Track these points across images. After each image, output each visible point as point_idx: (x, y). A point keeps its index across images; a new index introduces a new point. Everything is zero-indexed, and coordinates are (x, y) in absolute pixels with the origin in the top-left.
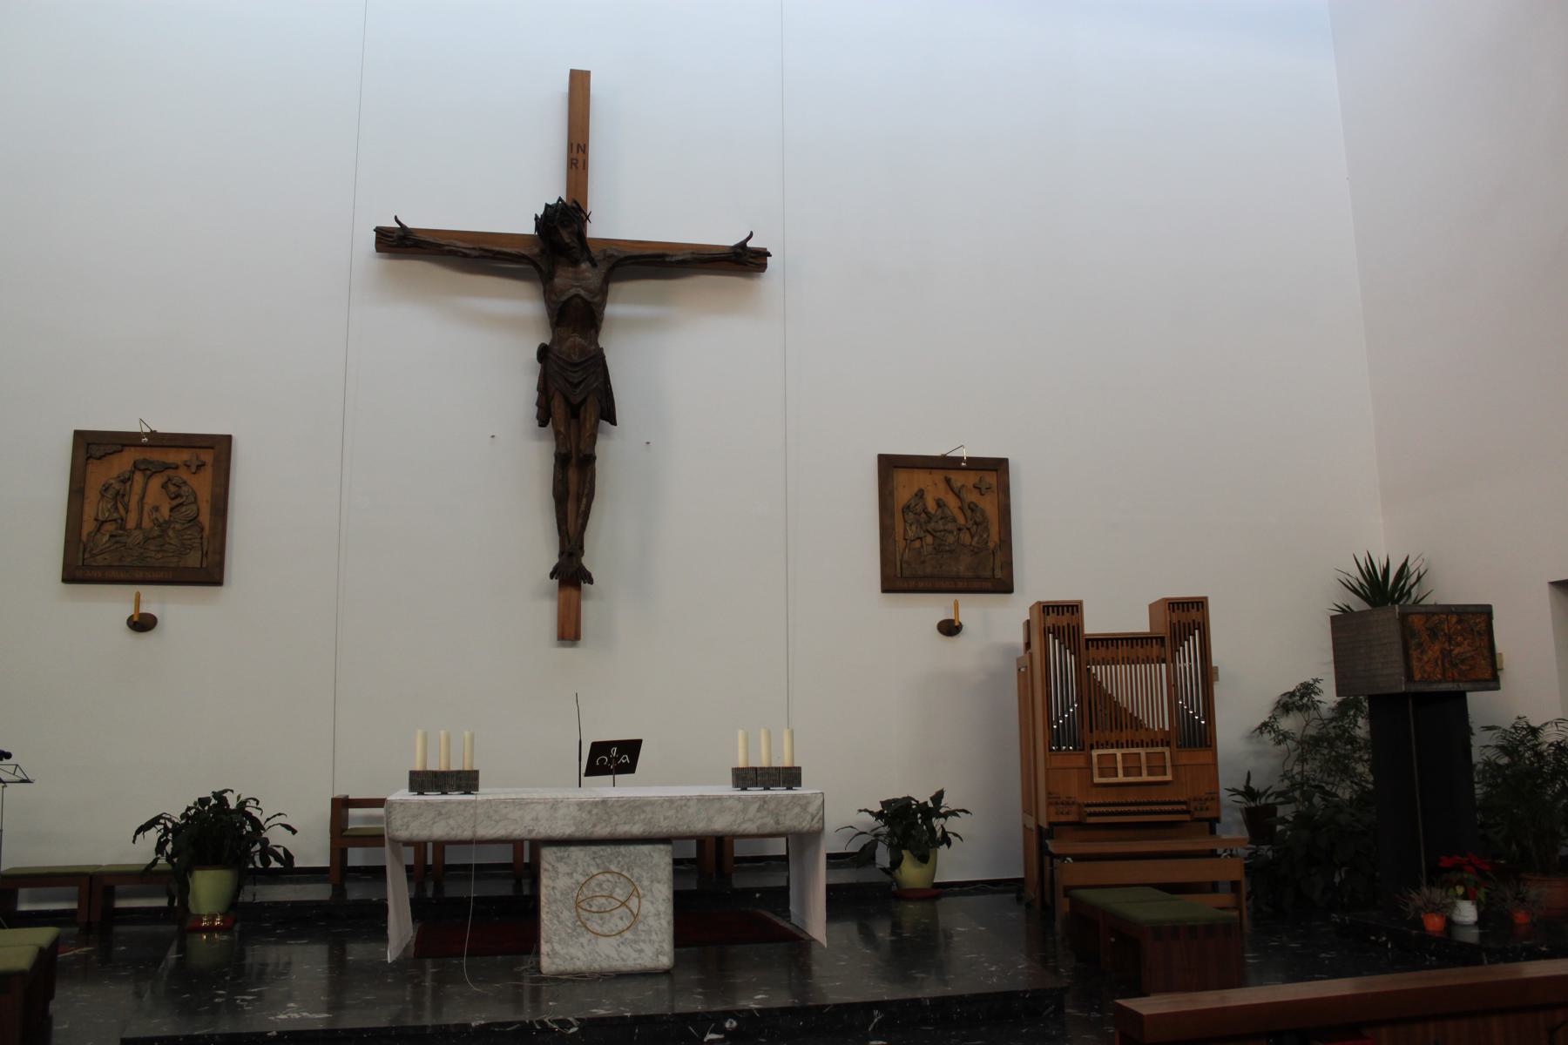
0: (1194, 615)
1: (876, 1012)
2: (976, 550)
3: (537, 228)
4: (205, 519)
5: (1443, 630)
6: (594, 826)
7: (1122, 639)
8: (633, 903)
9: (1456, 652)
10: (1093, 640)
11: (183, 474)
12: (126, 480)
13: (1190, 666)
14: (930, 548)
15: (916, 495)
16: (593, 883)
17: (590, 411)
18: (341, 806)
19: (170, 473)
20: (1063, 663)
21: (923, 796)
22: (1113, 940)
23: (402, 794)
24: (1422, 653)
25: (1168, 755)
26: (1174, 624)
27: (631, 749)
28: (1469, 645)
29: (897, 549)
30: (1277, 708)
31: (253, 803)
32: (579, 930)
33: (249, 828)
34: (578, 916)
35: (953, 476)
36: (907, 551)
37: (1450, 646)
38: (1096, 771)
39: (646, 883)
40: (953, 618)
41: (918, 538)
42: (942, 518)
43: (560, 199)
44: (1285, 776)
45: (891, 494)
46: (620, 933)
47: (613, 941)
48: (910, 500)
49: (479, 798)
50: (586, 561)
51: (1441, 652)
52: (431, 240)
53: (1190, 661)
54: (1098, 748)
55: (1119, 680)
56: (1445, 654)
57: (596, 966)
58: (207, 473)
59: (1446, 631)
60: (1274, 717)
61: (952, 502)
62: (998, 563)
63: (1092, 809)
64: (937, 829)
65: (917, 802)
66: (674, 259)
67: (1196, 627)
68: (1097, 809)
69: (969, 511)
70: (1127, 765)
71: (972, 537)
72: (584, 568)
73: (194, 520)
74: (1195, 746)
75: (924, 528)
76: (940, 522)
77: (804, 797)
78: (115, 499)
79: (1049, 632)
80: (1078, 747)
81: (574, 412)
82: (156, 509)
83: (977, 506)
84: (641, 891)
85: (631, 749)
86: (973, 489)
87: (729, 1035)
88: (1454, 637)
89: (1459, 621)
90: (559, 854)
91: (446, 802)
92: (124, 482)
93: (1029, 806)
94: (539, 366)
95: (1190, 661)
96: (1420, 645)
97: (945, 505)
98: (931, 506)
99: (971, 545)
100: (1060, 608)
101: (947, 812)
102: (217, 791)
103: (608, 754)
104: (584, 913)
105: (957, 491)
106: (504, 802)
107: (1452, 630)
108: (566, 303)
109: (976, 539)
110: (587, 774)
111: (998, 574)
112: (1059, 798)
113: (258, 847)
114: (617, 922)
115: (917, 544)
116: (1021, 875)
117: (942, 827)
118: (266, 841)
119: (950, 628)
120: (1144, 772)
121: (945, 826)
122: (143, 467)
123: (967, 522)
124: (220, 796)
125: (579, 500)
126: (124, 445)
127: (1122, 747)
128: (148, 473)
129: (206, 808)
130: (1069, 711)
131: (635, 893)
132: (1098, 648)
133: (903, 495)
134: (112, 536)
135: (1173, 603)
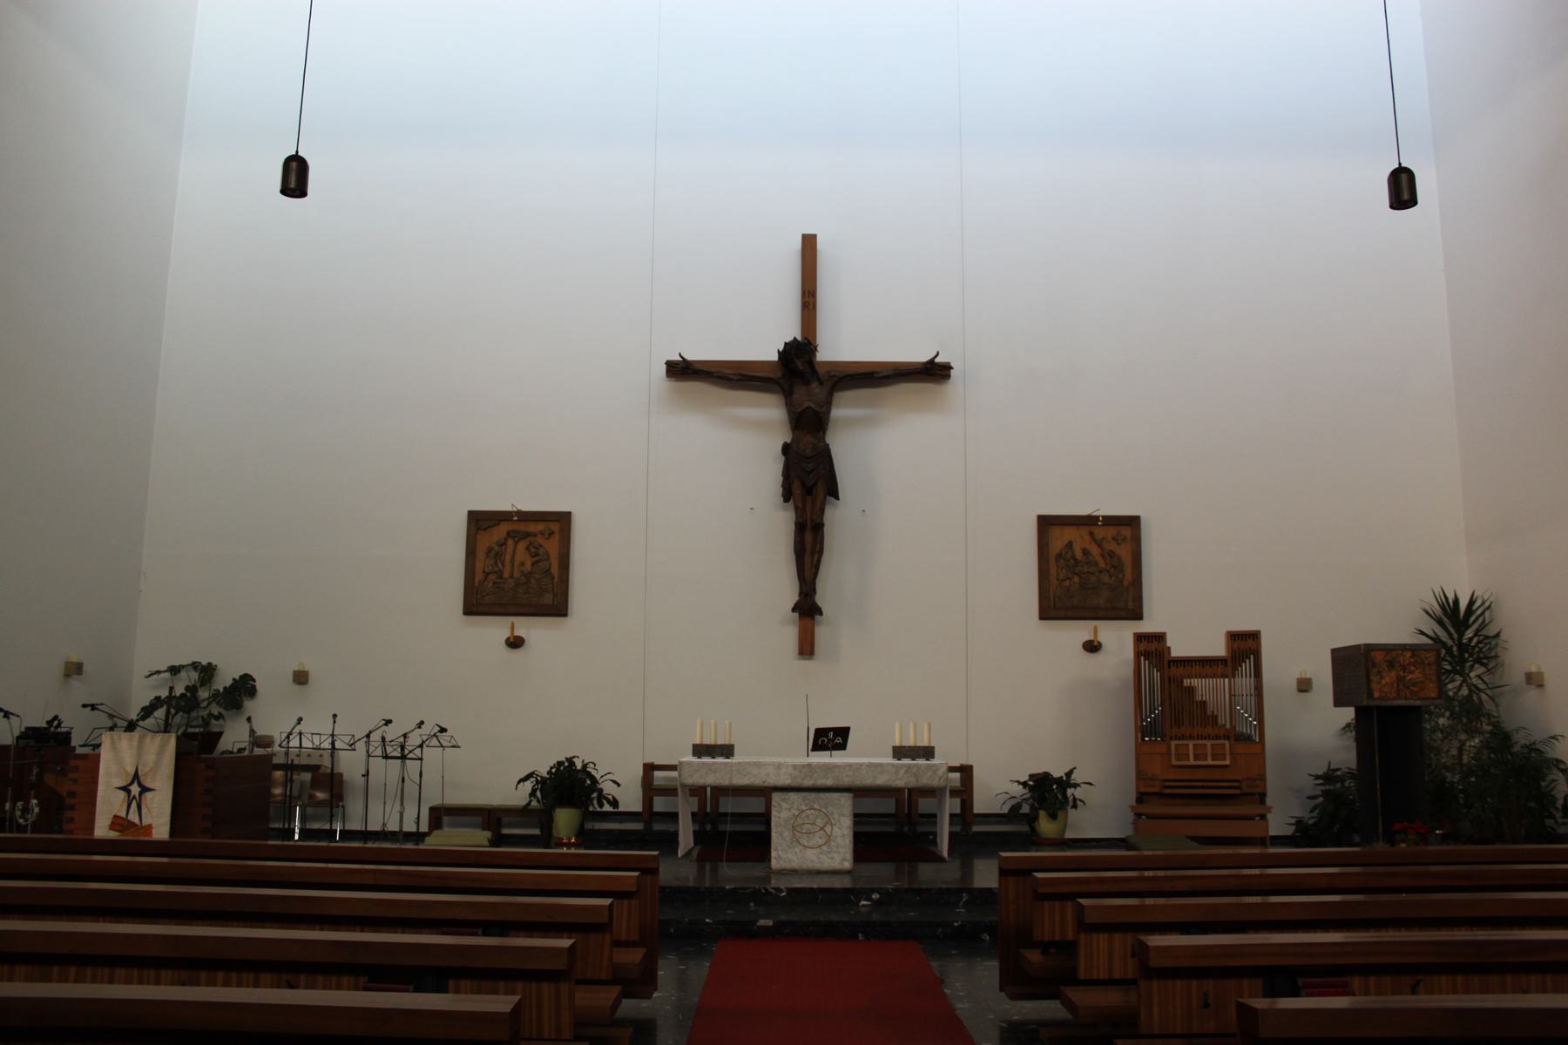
1: (964, 895)
3: (779, 358)
4: (555, 570)
6: (803, 780)
8: (828, 829)
9: (1408, 678)
11: (540, 540)
12: (503, 544)
15: (1067, 545)
16: (804, 815)
17: (820, 490)
18: (649, 768)
19: (531, 539)
20: (1151, 678)
21: (1058, 772)
23: (690, 758)
24: (1382, 678)
27: (843, 733)
28: (1419, 673)
31: (592, 765)
32: (794, 843)
33: (589, 782)
34: (794, 835)
35: (1095, 530)
39: (836, 816)
43: (795, 339)
46: (820, 847)
47: (814, 851)
49: (734, 761)
50: (820, 599)
52: (704, 369)
54: (1176, 739)
55: (1204, 687)
56: (1399, 679)
57: (805, 867)
58: (556, 537)
61: (1095, 550)
66: (881, 375)
71: (1110, 576)
72: (816, 604)
73: (548, 572)
77: (934, 765)
78: (495, 557)
81: (808, 491)
82: (523, 564)
84: (833, 822)
85: (843, 733)
87: (875, 903)
90: (783, 797)
91: (714, 763)
92: (501, 546)
94: (783, 458)
96: (1379, 673)
98: (1078, 554)
102: (568, 756)
103: (827, 737)
104: (798, 833)
106: (749, 763)
107: (1407, 662)
108: (804, 411)
109: (1113, 579)
110: (812, 750)
113: (595, 795)
114: (818, 839)
115: (1067, 583)
118: (601, 790)
119: (1092, 647)
120: (1209, 758)
122: (512, 535)
124: (570, 760)
125: (813, 554)
126: (500, 521)
127: (1194, 739)
128: (516, 539)
129: (562, 768)
131: (828, 822)
133: (1057, 545)
134: (494, 583)
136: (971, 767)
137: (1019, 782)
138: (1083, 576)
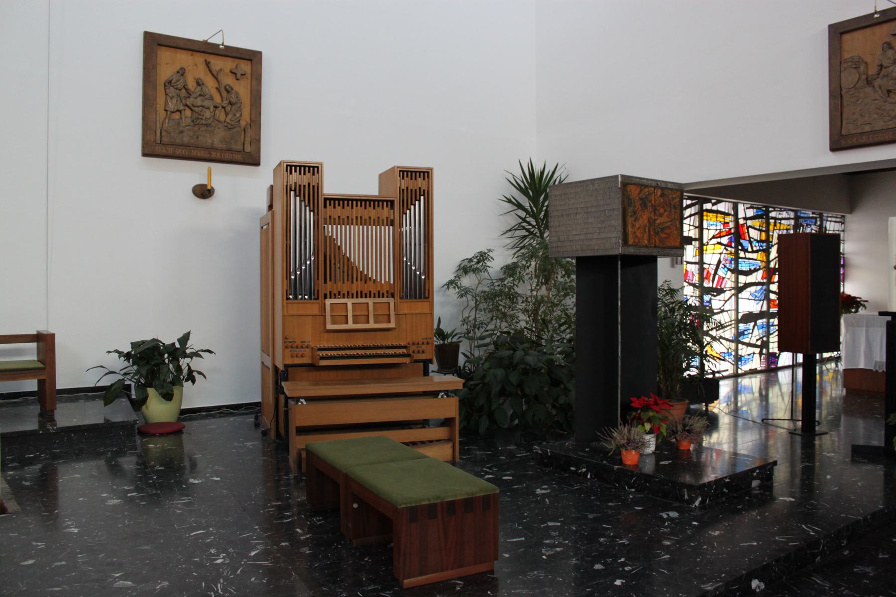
0: (420, 183)
2: (229, 126)
5: (651, 201)
7: (357, 200)
10: (330, 199)
13: (410, 230)
14: (189, 121)
20: (303, 220)
21: (169, 338)
22: (355, 506)
24: (635, 220)
25: (392, 305)
26: (403, 190)
29: (158, 119)
30: (459, 269)
35: (213, 60)
36: (167, 120)
37: (655, 216)
38: (328, 319)
40: (206, 183)
41: (178, 111)
42: (200, 95)
44: (465, 321)
45: (155, 67)
48: (172, 76)
51: (649, 220)
53: (410, 225)
56: (651, 222)
59: (653, 202)
60: (458, 277)
61: (210, 83)
62: (248, 140)
63: (324, 353)
64: (183, 367)
65: (164, 344)
67: (422, 193)
68: (329, 353)
69: (226, 93)
70: (356, 314)
71: (227, 114)
74: (415, 298)
75: (183, 101)
76: (199, 99)
79: (291, 190)
80: (313, 297)
83: (232, 89)
86: (230, 74)
88: (658, 208)
89: (662, 195)
93: (267, 346)
95: (410, 225)
97: (203, 84)
98: (191, 85)
99: (225, 122)
100: (302, 169)
101: (191, 353)
105: (215, 73)
109: (230, 117)
111: (248, 149)
112: (295, 342)
115: (177, 116)
116: (259, 400)
117: (188, 364)
121: (190, 364)
123: (222, 101)
130: (306, 264)
132: (335, 207)
133: (165, 72)
135: (403, 172)
136: (52, 336)
137: (120, 354)
138: (196, 109)
